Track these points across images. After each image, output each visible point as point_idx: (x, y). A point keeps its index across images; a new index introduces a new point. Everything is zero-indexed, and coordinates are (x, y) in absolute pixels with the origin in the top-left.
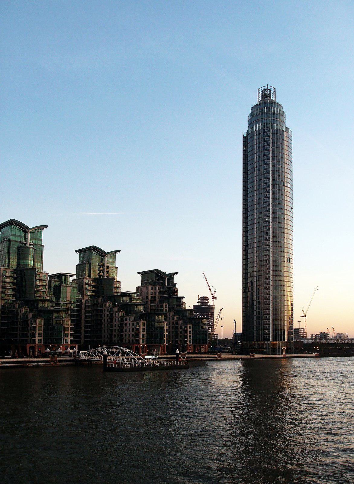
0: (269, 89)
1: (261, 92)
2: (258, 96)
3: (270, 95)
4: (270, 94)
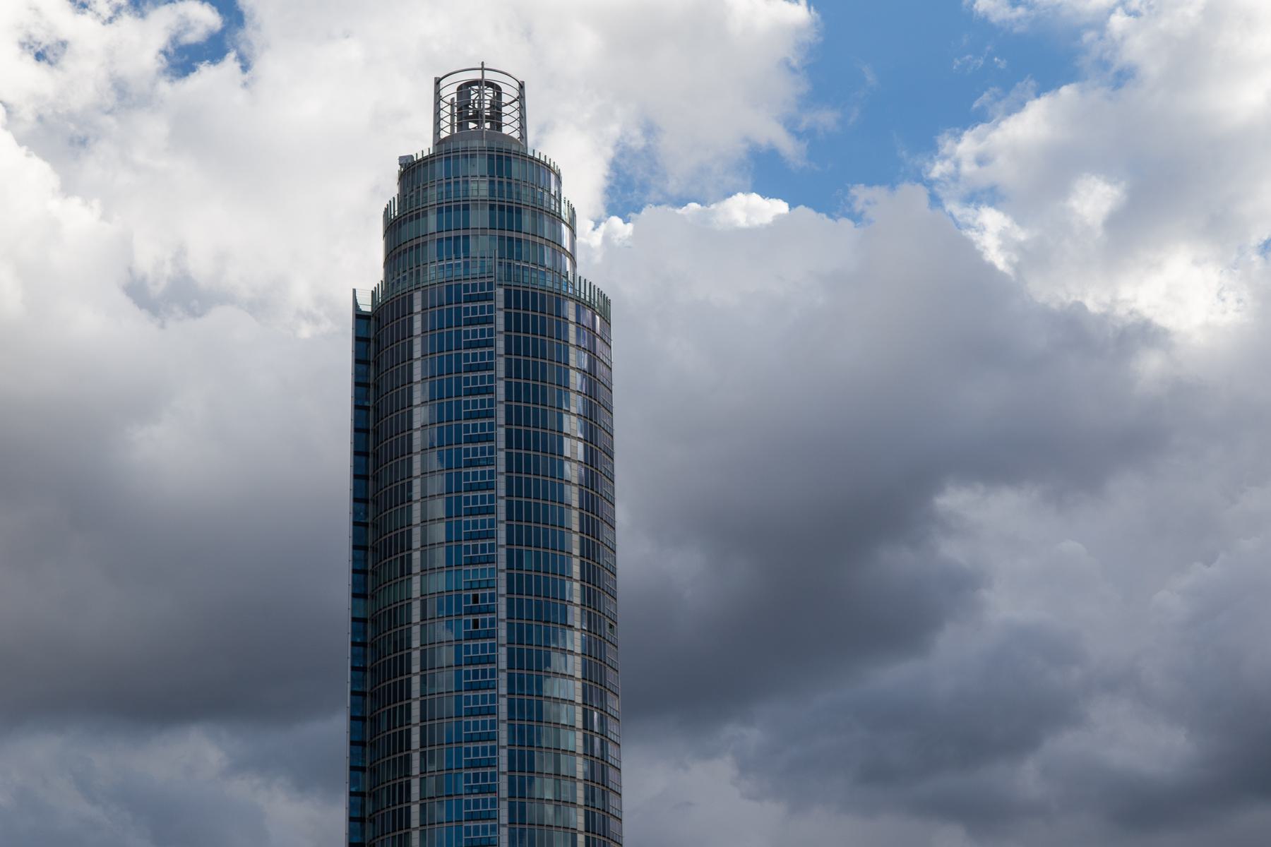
0: (490, 84)
1: (449, 92)
2: (438, 98)
3: (496, 117)
4: (497, 106)
